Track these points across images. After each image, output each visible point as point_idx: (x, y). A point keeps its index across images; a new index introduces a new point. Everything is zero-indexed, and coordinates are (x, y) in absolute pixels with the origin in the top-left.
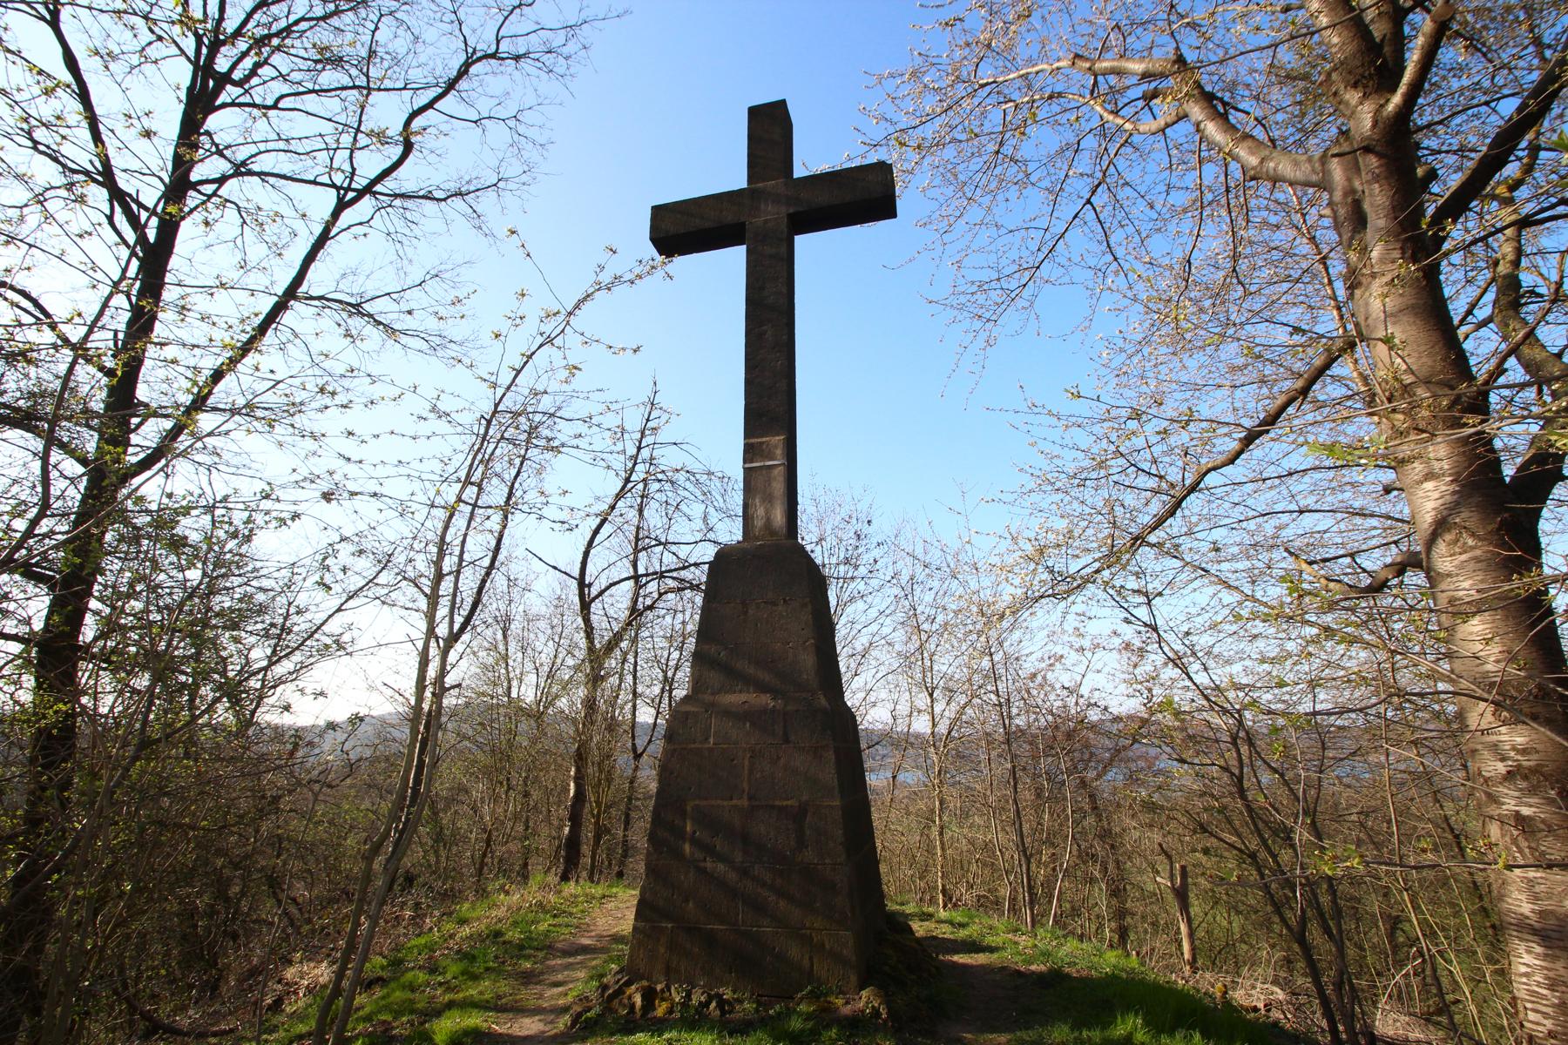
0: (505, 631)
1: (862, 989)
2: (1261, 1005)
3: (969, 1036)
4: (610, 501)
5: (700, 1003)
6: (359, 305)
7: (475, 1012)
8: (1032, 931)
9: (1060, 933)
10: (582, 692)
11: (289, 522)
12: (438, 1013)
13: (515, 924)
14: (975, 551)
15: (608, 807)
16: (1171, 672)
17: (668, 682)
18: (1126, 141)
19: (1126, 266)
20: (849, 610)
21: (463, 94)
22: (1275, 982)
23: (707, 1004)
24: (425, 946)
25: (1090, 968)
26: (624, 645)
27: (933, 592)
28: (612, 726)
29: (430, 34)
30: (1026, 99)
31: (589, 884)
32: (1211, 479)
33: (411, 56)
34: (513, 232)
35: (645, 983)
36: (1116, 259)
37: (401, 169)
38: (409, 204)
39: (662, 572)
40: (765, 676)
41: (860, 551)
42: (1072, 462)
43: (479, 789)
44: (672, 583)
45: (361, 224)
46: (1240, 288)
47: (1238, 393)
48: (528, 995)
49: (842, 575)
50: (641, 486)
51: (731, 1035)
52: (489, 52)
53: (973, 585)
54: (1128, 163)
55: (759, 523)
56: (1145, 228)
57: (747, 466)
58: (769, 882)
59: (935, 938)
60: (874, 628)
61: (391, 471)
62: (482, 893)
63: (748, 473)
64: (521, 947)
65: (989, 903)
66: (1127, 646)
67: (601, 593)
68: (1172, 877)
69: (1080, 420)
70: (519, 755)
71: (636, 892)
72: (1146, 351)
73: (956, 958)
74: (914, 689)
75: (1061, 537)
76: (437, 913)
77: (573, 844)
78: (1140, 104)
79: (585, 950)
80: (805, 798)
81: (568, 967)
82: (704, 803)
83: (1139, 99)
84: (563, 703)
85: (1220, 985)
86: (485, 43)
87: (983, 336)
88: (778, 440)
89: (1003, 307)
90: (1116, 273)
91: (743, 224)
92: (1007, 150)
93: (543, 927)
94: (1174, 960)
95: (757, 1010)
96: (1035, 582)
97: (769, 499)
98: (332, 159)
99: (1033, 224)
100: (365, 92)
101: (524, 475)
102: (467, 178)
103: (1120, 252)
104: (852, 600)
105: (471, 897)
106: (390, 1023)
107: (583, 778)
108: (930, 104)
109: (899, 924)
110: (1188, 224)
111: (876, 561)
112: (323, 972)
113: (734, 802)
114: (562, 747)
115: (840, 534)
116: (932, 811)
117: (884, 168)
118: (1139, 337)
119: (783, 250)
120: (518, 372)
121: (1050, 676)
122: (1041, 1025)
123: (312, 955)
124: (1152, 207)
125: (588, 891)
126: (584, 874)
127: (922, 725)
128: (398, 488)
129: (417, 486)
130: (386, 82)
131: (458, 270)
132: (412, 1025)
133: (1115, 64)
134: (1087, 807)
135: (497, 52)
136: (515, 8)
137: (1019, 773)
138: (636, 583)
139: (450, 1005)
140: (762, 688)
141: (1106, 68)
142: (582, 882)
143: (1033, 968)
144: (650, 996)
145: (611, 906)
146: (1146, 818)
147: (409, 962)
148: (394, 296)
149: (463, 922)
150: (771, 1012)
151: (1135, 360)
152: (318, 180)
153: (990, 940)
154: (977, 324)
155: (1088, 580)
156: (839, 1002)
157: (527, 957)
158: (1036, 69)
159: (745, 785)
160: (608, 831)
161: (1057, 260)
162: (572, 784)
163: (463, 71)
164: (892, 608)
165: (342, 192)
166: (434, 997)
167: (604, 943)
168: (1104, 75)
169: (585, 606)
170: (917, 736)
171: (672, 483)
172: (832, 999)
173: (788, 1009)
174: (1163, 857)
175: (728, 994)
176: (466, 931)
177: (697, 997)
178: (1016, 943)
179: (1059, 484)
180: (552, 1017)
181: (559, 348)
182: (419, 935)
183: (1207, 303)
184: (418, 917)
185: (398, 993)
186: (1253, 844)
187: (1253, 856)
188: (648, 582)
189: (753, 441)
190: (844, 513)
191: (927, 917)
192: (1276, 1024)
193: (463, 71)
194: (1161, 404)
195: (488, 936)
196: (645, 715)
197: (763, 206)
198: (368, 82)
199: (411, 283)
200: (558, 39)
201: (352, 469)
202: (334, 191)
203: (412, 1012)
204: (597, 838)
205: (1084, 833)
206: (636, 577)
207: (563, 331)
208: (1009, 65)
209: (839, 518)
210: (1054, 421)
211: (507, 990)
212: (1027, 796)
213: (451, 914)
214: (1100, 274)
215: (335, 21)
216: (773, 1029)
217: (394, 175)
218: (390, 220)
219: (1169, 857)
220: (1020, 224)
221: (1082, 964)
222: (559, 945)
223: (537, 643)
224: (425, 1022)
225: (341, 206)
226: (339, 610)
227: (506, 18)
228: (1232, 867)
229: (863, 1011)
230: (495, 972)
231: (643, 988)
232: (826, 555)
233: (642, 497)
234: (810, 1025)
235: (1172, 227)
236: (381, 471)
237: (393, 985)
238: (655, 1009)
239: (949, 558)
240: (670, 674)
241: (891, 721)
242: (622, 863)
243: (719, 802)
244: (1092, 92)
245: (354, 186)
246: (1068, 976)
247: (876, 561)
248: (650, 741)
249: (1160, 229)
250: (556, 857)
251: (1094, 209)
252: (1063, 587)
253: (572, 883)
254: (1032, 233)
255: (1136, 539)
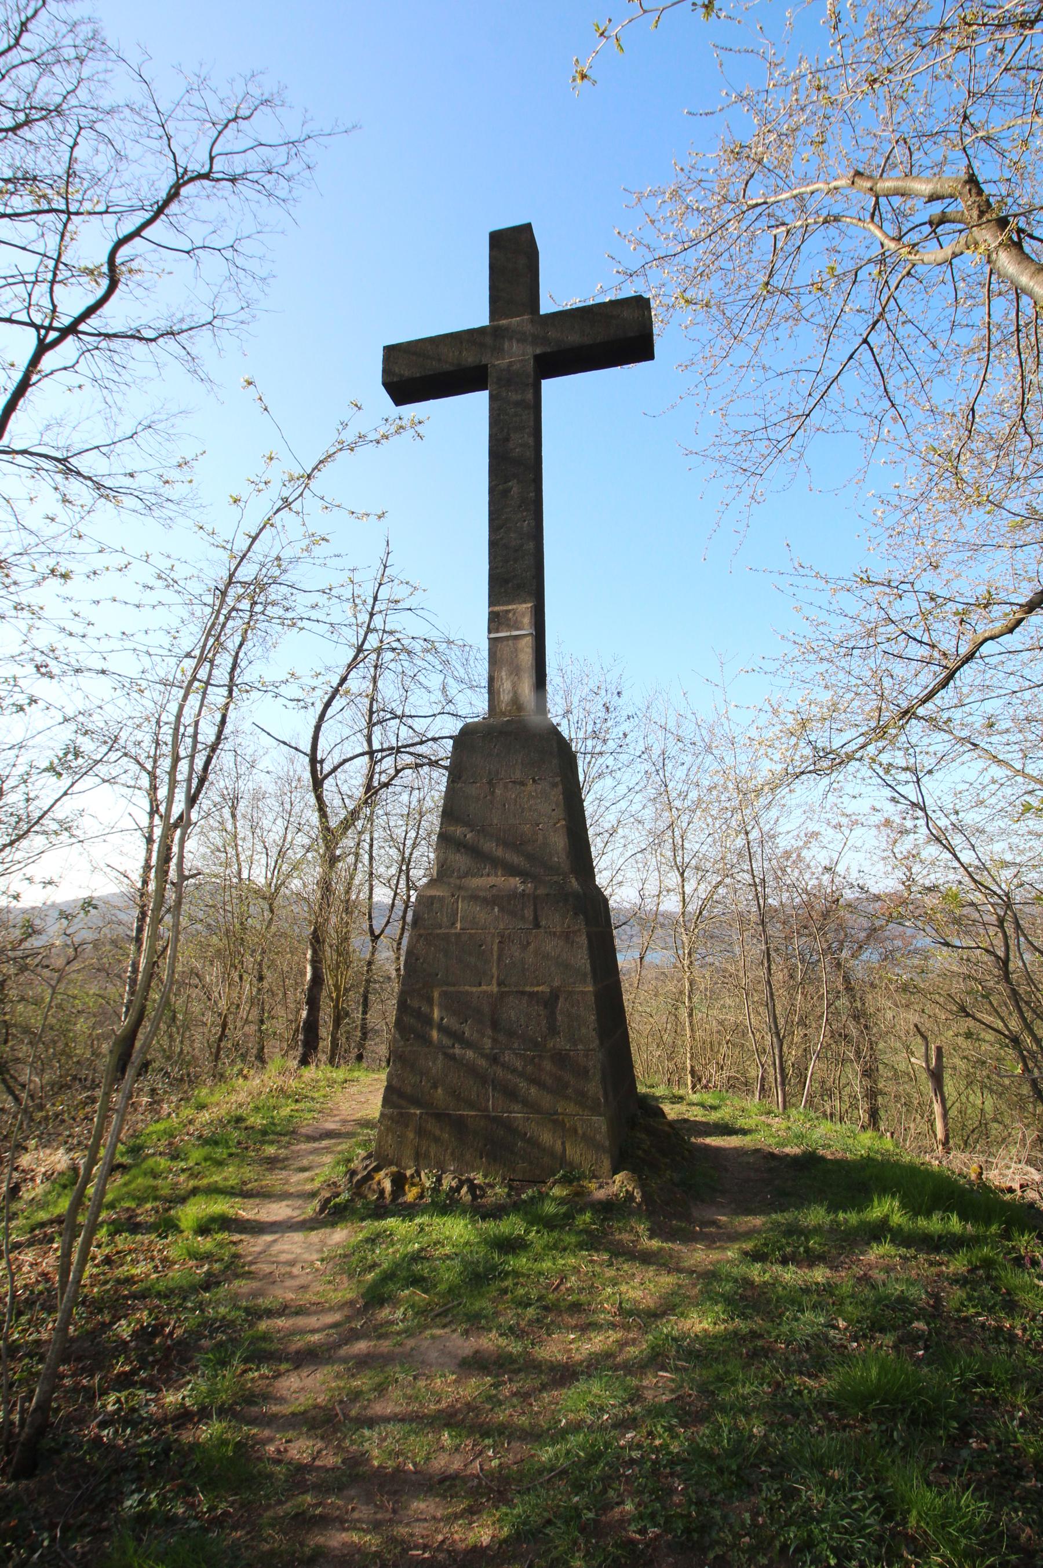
0: (234, 808)
1: (615, 1173)
2: (1016, 1186)
3: (724, 1218)
4: (342, 671)
5: (451, 1188)
6: (65, 460)
7: (220, 1198)
8: (784, 1113)
9: (813, 1115)
10: (317, 872)
11: (26, 707)
12: (183, 1200)
13: (257, 1109)
14: (733, 726)
15: (346, 990)
16: (932, 851)
17: (405, 862)
18: (909, 273)
19: (904, 413)
20: (596, 787)
21: (172, 219)
22: (1029, 1162)
23: (458, 1189)
24: (165, 1132)
25: (845, 1150)
26: (359, 824)
27: (685, 767)
28: (349, 908)
29: (133, 151)
30: (799, 223)
31: (329, 1068)
32: (985, 649)
33: (112, 175)
34: (250, 383)
35: (394, 1169)
36: (893, 405)
37: (107, 306)
38: (116, 344)
39: (399, 748)
40: (516, 859)
41: (609, 724)
42: (838, 628)
43: (212, 974)
44: (408, 759)
45: (65, 369)
46: (1027, 438)
47: (1020, 554)
48: (273, 1180)
49: (589, 749)
50: (374, 656)
51: (483, 1218)
52: (203, 172)
53: (729, 760)
54: (911, 296)
55: (505, 697)
56: (926, 370)
57: (492, 636)
58: (520, 1069)
59: (686, 1121)
60: (623, 804)
61: (115, 644)
62: (220, 1077)
63: (493, 642)
64: (264, 1133)
65: (738, 1085)
66: (888, 823)
67: (335, 769)
68: (927, 1060)
69: (849, 584)
70: (251, 939)
71: (384, 1076)
72: (923, 507)
73: (709, 1141)
74: (664, 868)
75: (825, 710)
76: (174, 1099)
77: (311, 1028)
78: (927, 229)
79: (329, 1134)
80: (556, 984)
81: (315, 1151)
82: (452, 989)
83: (924, 224)
84: (295, 884)
85: (975, 1166)
86: (197, 163)
87: (748, 491)
88: (524, 609)
89: (770, 459)
90: (895, 420)
91: (486, 366)
92: (778, 281)
93: (285, 1112)
94: (927, 1142)
95: (509, 1195)
96: (797, 757)
97: (516, 671)
98: (30, 295)
99: (804, 366)
100: (64, 217)
101: (249, 644)
102: (179, 315)
103: (899, 399)
104: (600, 775)
105: (209, 1082)
106: (134, 1210)
107: (320, 962)
108: (693, 227)
109: (649, 1108)
110: (974, 367)
111: (625, 735)
112: (59, 1159)
113: (484, 988)
114: (297, 930)
115: (588, 706)
116: (681, 993)
117: (641, 304)
118: (915, 493)
119: (530, 396)
120: (254, 539)
121: (804, 853)
122: (797, 1209)
123: (46, 1142)
124: (934, 347)
125: (329, 1075)
126: (324, 1058)
127: (671, 904)
128: (127, 665)
129: (146, 662)
130: (85, 203)
131: (173, 420)
132: (157, 1212)
133: (900, 184)
134: (841, 988)
135: (210, 171)
136: (230, 121)
137: (773, 954)
138: (371, 758)
139: (194, 1192)
140: (512, 871)
141: (889, 189)
142: (322, 1067)
143: (787, 1150)
144: (399, 1182)
145: (353, 1090)
146: (902, 998)
147: (149, 1148)
148: (104, 449)
149: (202, 1107)
150: (524, 1196)
151: (912, 518)
152: (15, 317)
153: (742, 1123)
154: (740, 479)
155: (850, 757)
156: (592, 1186)
157: (272, 1143)
158: (809, 189)
159: (494, 970)
160: (347, 1014)
161: (829, 406)
162: (309, 968)
163: (173, 194)
164: (642, 784)
165: (43, 332)
166: (176, 1184)
167: (349, 1128)
168: (887, 196)
169: (317, 784)
170: (666, 915)
171: (409, 653)
172: (585, 1183)
173: (540, 1193)
174: (919, 1039)
175: (479, 1179)
176: (205, 1116)
177: (448, 1182)
178: (769, 1125)
179: (824, 653)
180: (300, 1202)
181: (298, 513)
182: (157, 1121)
183: (990, 456)
184: (155, 1104)
185: (140, 1180)
186: (1014, 1024)
187: (1015, 1041)
188: (383, 758)
189: (497, 609)
190: (592, 685)
191: (678, 1099)
192: (1032, 1205)
193: (173, 194)
194: (936, 567)
195: (229, 1122)
196: (382, 895)
197: (506, 345)
198: (67, 204)
199: (120, 434)
200: (278, 157)
201: (73, 644)
202: (33, 330)
203: (156, 1199)
204: (337, 1022)
205: (837, 1013)
206: (371, 753)
207: (301, 495)
208: (781, 183)
209: (586, 690)
210: (821, 584)
211: (252, 1175)
212: (779, 976)
213: (188, 1099)
214: (877, 422)
215: (24, 132)
216: (526, 1213)
217: (98, 312)
218: (97, 364)
219: (924, 1038)
220: (790, 366)
221: (838, 1146)
222: (303, 1131)
223: (265, 822)
224: (170, 1208)
225: (43, 348)
226: (65, 794)
227: (220, 133)
228: (989, 1045)
229: (616, 1195)
230: (239, 1156)
231: (393, 1174)
232: (573, 730)
233: (376, 667)
234: (563, 1209)
235: (957, 370)
236: (105, 645)
237: (134, 1171)
238: (404, 1194)
239: (704, 732)
240: (407, 855)
241: (638, 901)
242: (361, 1046)
243: (467, 988)
244: (873, 215)
245: (55, 324)
246: (822, 1159)
247: (625, 735)
248: (388, 922)
249: (941, 372)
250: (294, 1039)
251: (871, 349)
252: (825, 764)
253: (313, 1067)
254: (804, 376)
255: (906, 712)
